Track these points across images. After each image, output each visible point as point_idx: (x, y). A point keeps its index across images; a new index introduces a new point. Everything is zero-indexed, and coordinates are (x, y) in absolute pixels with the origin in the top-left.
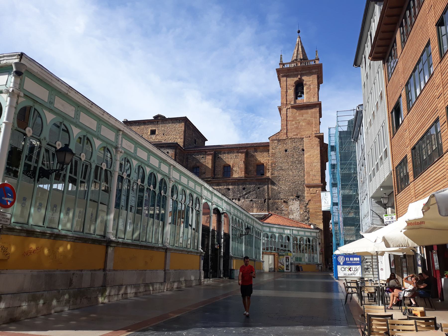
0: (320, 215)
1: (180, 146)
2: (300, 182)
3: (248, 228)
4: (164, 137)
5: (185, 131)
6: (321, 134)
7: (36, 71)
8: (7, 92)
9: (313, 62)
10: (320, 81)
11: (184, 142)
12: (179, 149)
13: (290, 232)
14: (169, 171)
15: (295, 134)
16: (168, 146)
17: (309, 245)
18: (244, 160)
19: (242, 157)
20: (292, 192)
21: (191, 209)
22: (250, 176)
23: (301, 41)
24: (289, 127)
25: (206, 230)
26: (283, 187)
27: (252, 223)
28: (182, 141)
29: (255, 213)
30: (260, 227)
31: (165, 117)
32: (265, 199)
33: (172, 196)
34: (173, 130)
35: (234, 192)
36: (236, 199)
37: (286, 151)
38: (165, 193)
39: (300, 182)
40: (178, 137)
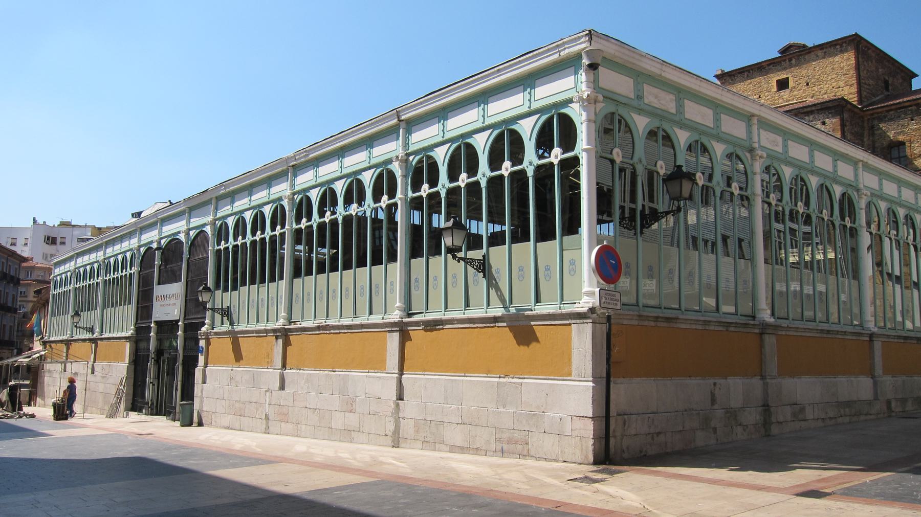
1: (851, 104)
4: (809, 91)
5: (858, 67)
8: (581, 99)
11: (859, 92)
12: (850, 110)
14: (856, 175)
16: (822, 109)
28: (854, 89)
31: (804, 46)
34: (828, 69)
40: (841, 84)
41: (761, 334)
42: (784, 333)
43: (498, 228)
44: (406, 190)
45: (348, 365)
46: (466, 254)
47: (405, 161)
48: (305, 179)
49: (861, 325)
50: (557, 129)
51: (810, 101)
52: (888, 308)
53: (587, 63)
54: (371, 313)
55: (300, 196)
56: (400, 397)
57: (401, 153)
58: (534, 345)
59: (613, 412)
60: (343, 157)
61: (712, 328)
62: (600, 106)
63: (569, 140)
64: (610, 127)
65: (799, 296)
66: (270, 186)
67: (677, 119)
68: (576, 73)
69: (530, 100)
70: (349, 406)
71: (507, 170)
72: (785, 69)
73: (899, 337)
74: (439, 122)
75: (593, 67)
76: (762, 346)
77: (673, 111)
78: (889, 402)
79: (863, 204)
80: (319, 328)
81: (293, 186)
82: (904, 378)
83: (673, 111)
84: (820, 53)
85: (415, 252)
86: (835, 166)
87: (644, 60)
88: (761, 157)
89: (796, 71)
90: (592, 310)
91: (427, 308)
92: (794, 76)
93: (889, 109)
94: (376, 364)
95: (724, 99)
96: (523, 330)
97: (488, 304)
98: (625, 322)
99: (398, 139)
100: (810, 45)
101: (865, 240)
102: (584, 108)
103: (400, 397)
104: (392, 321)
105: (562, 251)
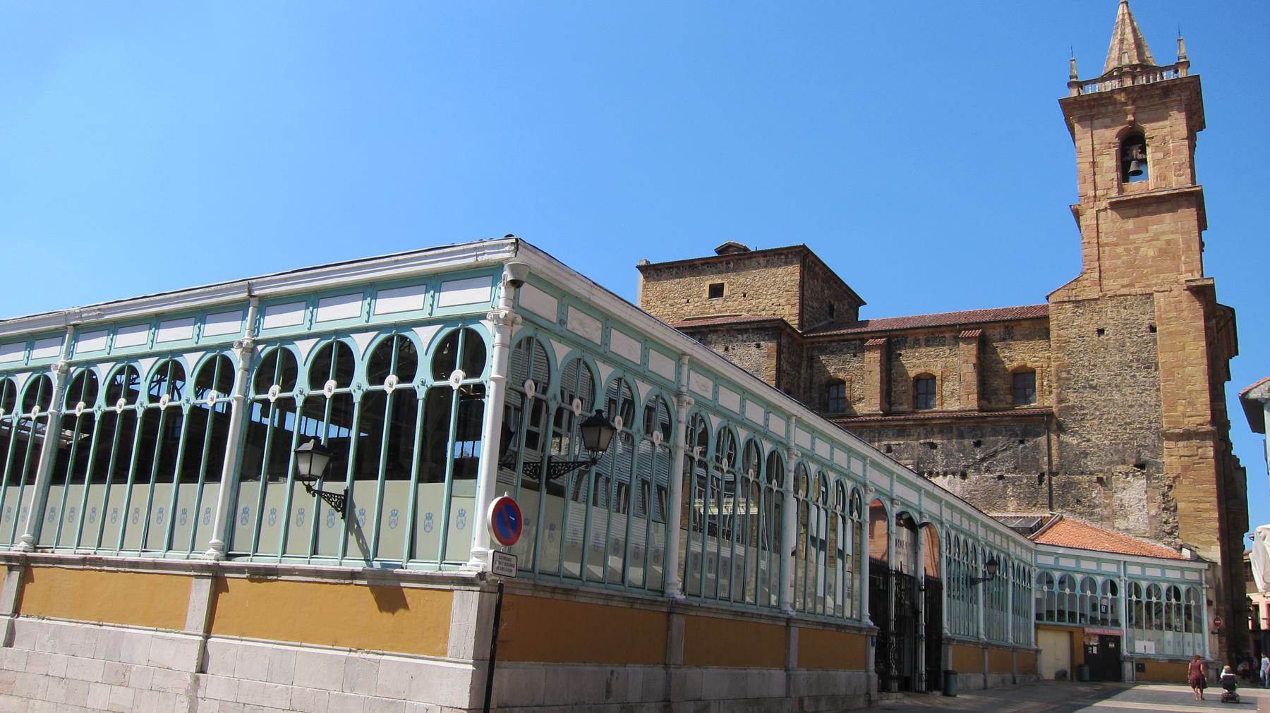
0: (1209, 519)
2: (1146, 424)
3: (992, 563)
4: (746, 305)
5: (802, 285)
6: (1206, 282)
7: (539, 267)
8: (497, 317)
9: (1172, 72)
10: (1196, 123)
11: (801, 314)
12: (789, 334)
13: (1119, 568)
14: (788, 431)
15: (1126, 281)
16: (757, 329)
17: (1178, 608)
18: (974, 360)
19: (968, 351)
20: (1125, 451)
21: (840, 519)
22: (994, 405)
23: (1130, 15)
24: (1106, 263)
25: (879, 569)
26: (1092, 438)
27: (1005, 545)
28: (796, 310)
29: (1013, 511)
30: (1027, 557)
31: (745, 249)
32: (1043, 474)
33: (796, 492)
34: (770, 281)
35: (948, 455)
36: (954, 474)
37: (1101, 332)
38: (780, 485)
39: (1146, 424)
40: (783, 301)
41: (669, 613)
42: (693, 613)
43: (344, 433)
44: (248, 388)
45: (123, 618)
46: (321, 485)
47: (251, 351)
48: (90, 348)
49: (779, 607)
50: (462, 347)
51: (746, 316)
52: (809, 582)
53: (510, 278)
54: (170, 548)
55: (80, 370)
56: (202, 669)
57: (246, 339)
58: (401, 612)
59: (493, 704)
60: (158, 328)
61: (615, 604)
62: (517, 328)
63: (475, 362)
64: (526, 350)
65: (714, 559)
66: (31, 347)
67: (601, 350)
68: (494, 284)
69: (432, 306)
70: (120, 676)
71: (391, 385)
72: (721, 272)
73: (818, 623)
74: (307, 308)
75: (516, 284)
76: (668, 628)
77: (598, 341)
78: (801, 700)
79: (792, 466)
80: (84, 561)
81: (70, 352)
82: (820, 671)
83: (598, 341)
84: (762, 261)
85: (248, 471)
86: (767, 420)
87: (573, 279)
88: (689, 403)
89: (732, 277)
90: (482, 575)
91: (256, 549)
92: (732, 282)
93: (832, 340)
94: (171, 619)
95: (656, 333)
96: (389, 592)
97: (344, 554)
98: (518, 592)
99: (244, 318)
100: (753, 249)
101: (791, 507)
102: (500, 329)
103: (202, 669)
104: (204, 562)
105: (450, 496)
